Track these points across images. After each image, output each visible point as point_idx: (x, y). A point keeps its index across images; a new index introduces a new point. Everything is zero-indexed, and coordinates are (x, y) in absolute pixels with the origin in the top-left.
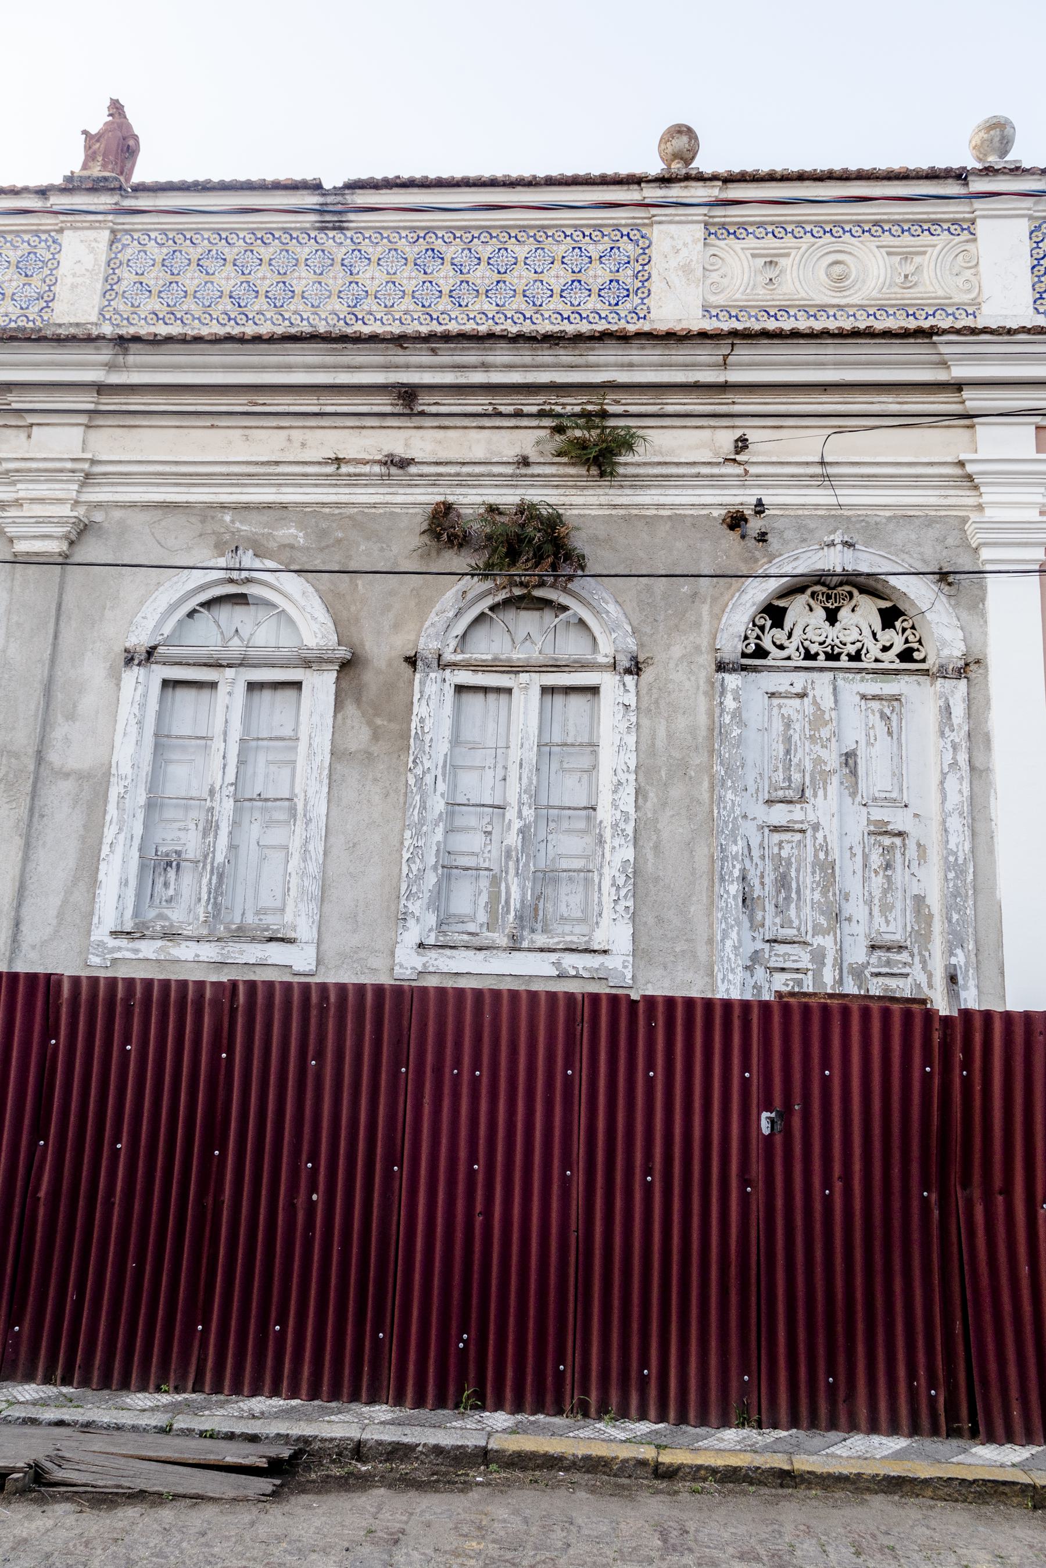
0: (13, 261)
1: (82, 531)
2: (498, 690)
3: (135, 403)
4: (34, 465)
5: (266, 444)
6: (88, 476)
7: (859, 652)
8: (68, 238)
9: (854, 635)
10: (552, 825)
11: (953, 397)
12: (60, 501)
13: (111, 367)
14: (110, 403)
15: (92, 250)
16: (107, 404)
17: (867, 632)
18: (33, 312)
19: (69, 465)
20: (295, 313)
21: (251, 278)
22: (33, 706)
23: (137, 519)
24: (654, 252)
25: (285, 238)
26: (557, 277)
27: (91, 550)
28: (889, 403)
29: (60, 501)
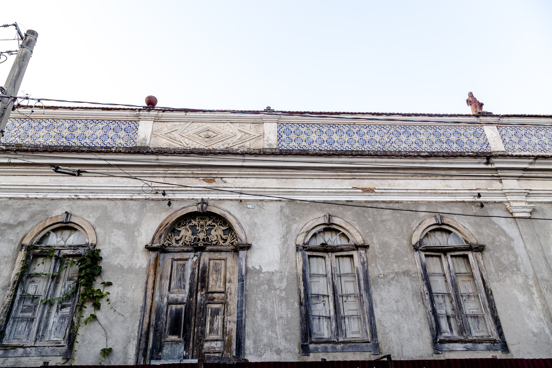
0: (123, 128)
1: (534, 211)
2: (322, 257)
3: (534, 174)
4: (514, 191)
5: (347, 184)
6: (528, 194)
7: (217, 243)
8: (141, 123)
9: (215, 238)
10: (345, 299)
11: (495, 172)
12: (522, 201)
13: (531, 163)
14: (527, 174)
15: (494, 131)
16: (526, 174)
17: (219, 237)
18: (484, 147)
19: (524, 191)
20: (97, 143)
21: (115, 133)
22: (544, 265)
23: (545, 207)
24: (139, 128)
25: (52, 121)
26: (99, 133)
27: (535, 216)
28: (443, 172)
29: (522, 201)
